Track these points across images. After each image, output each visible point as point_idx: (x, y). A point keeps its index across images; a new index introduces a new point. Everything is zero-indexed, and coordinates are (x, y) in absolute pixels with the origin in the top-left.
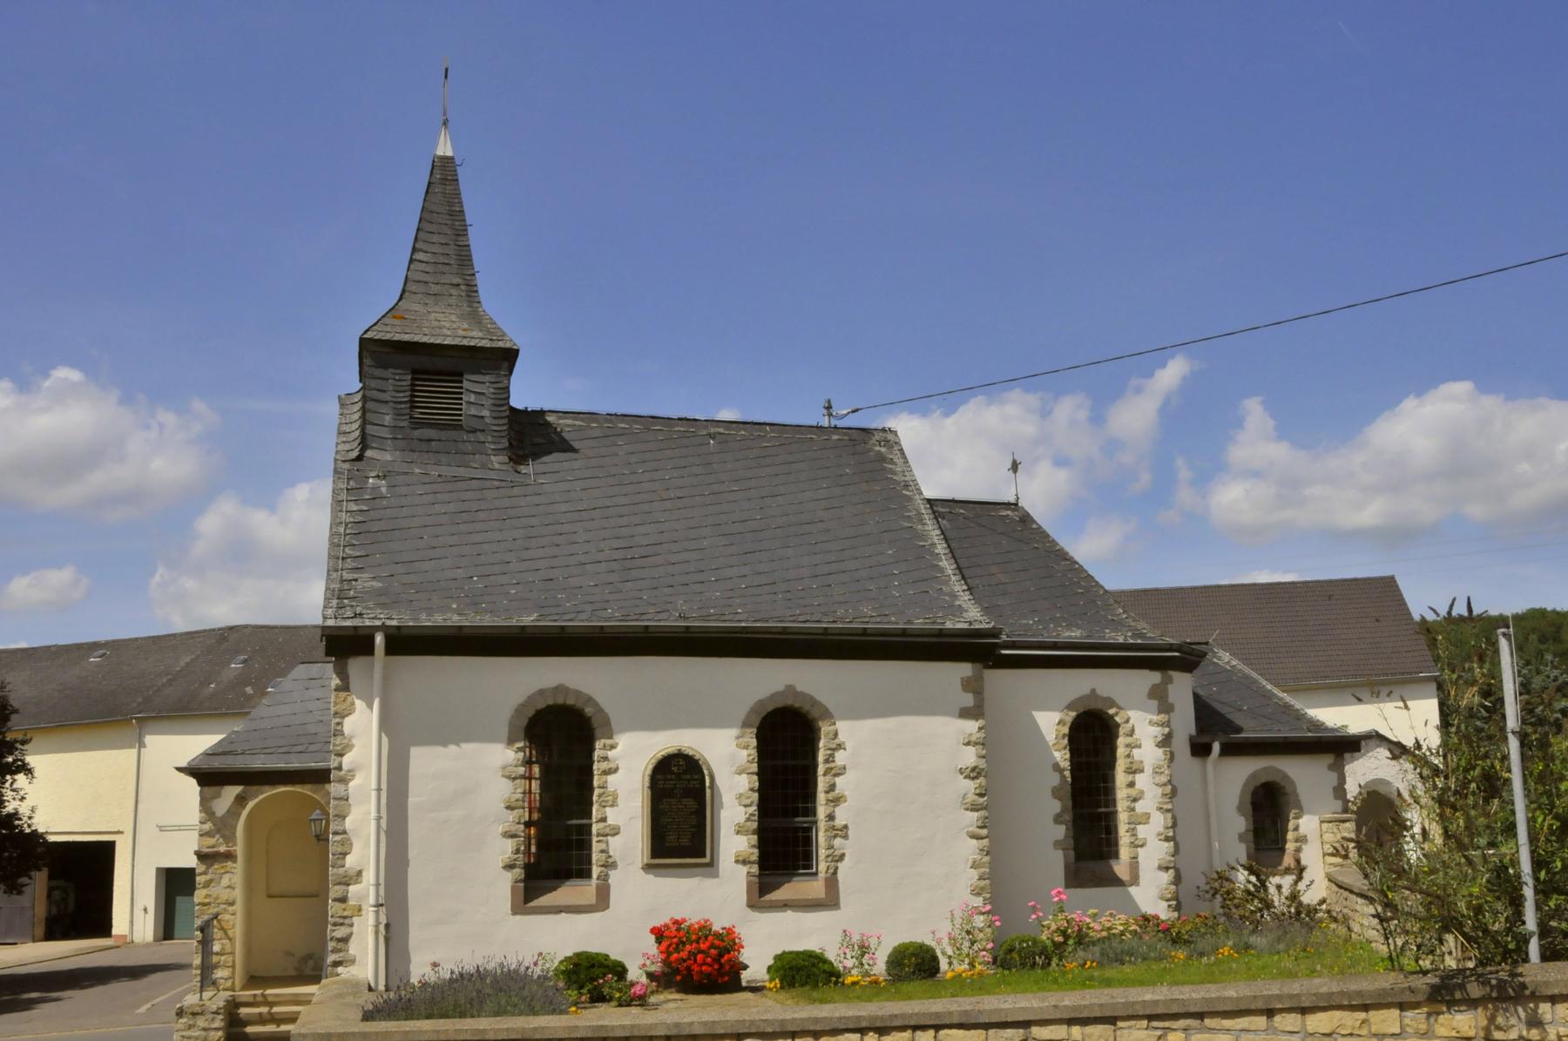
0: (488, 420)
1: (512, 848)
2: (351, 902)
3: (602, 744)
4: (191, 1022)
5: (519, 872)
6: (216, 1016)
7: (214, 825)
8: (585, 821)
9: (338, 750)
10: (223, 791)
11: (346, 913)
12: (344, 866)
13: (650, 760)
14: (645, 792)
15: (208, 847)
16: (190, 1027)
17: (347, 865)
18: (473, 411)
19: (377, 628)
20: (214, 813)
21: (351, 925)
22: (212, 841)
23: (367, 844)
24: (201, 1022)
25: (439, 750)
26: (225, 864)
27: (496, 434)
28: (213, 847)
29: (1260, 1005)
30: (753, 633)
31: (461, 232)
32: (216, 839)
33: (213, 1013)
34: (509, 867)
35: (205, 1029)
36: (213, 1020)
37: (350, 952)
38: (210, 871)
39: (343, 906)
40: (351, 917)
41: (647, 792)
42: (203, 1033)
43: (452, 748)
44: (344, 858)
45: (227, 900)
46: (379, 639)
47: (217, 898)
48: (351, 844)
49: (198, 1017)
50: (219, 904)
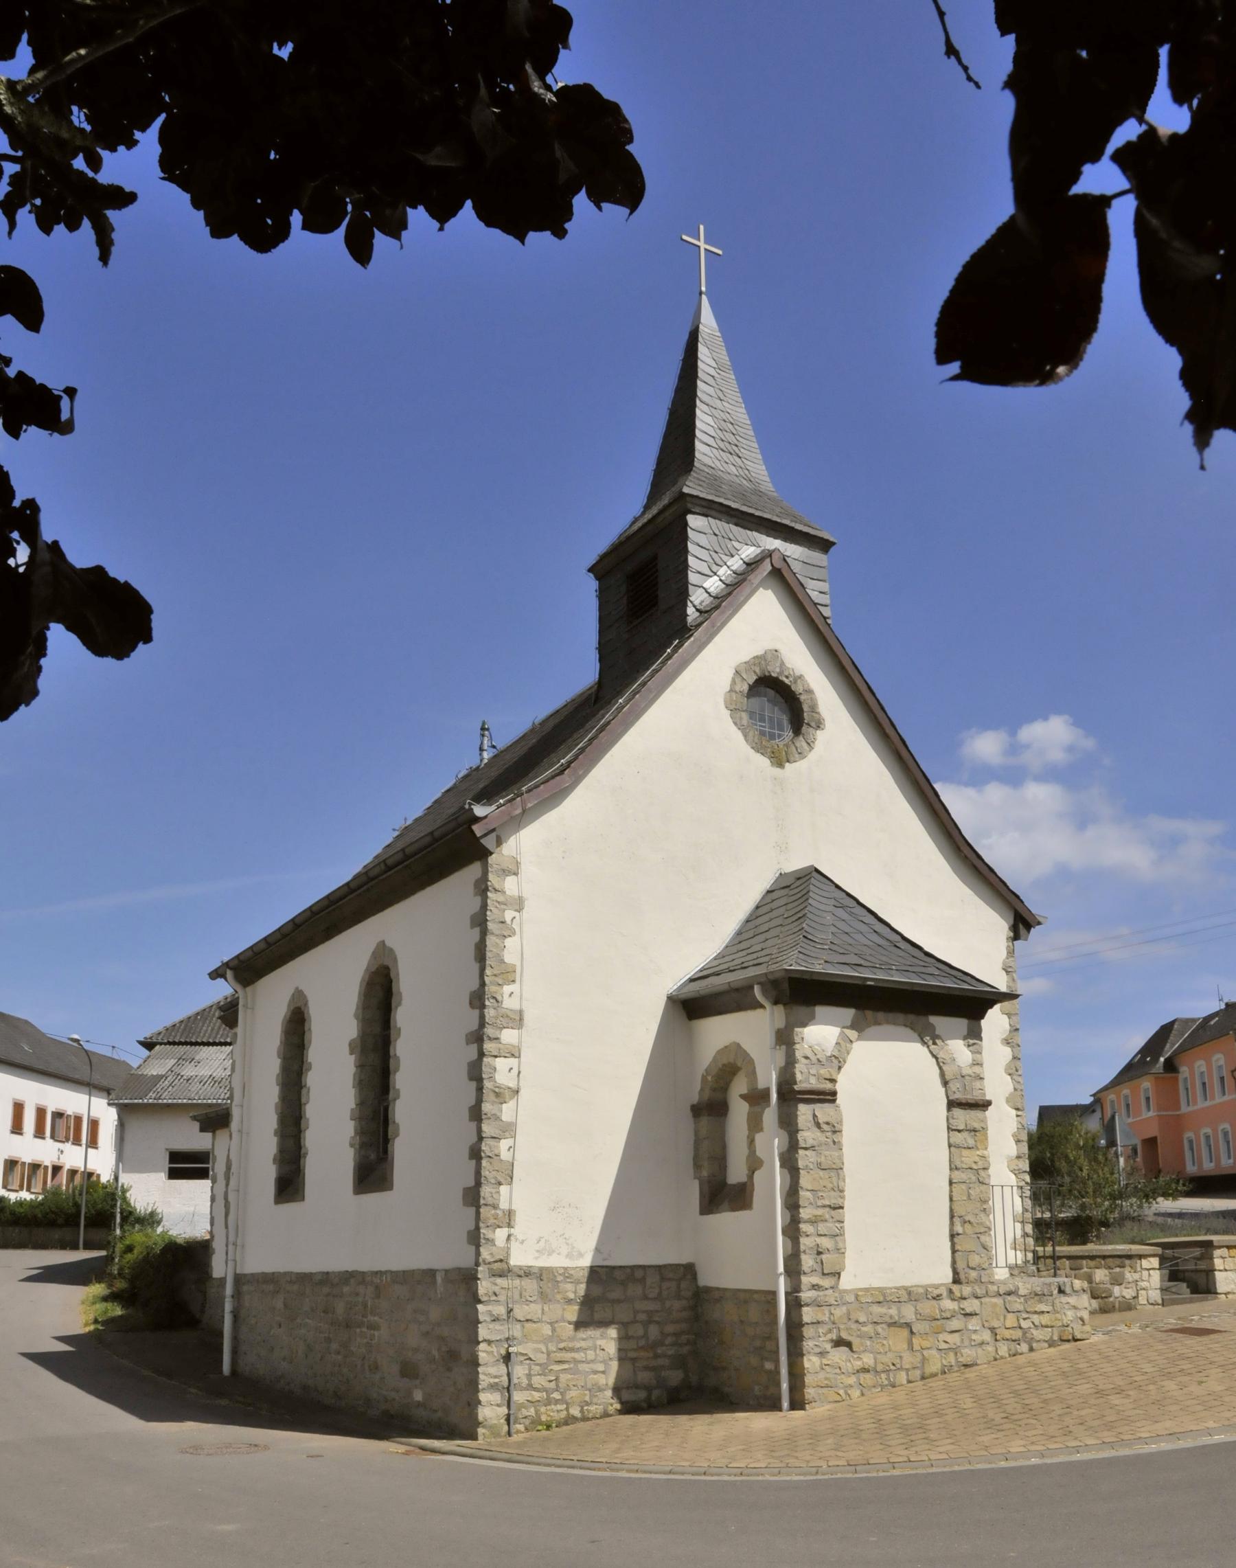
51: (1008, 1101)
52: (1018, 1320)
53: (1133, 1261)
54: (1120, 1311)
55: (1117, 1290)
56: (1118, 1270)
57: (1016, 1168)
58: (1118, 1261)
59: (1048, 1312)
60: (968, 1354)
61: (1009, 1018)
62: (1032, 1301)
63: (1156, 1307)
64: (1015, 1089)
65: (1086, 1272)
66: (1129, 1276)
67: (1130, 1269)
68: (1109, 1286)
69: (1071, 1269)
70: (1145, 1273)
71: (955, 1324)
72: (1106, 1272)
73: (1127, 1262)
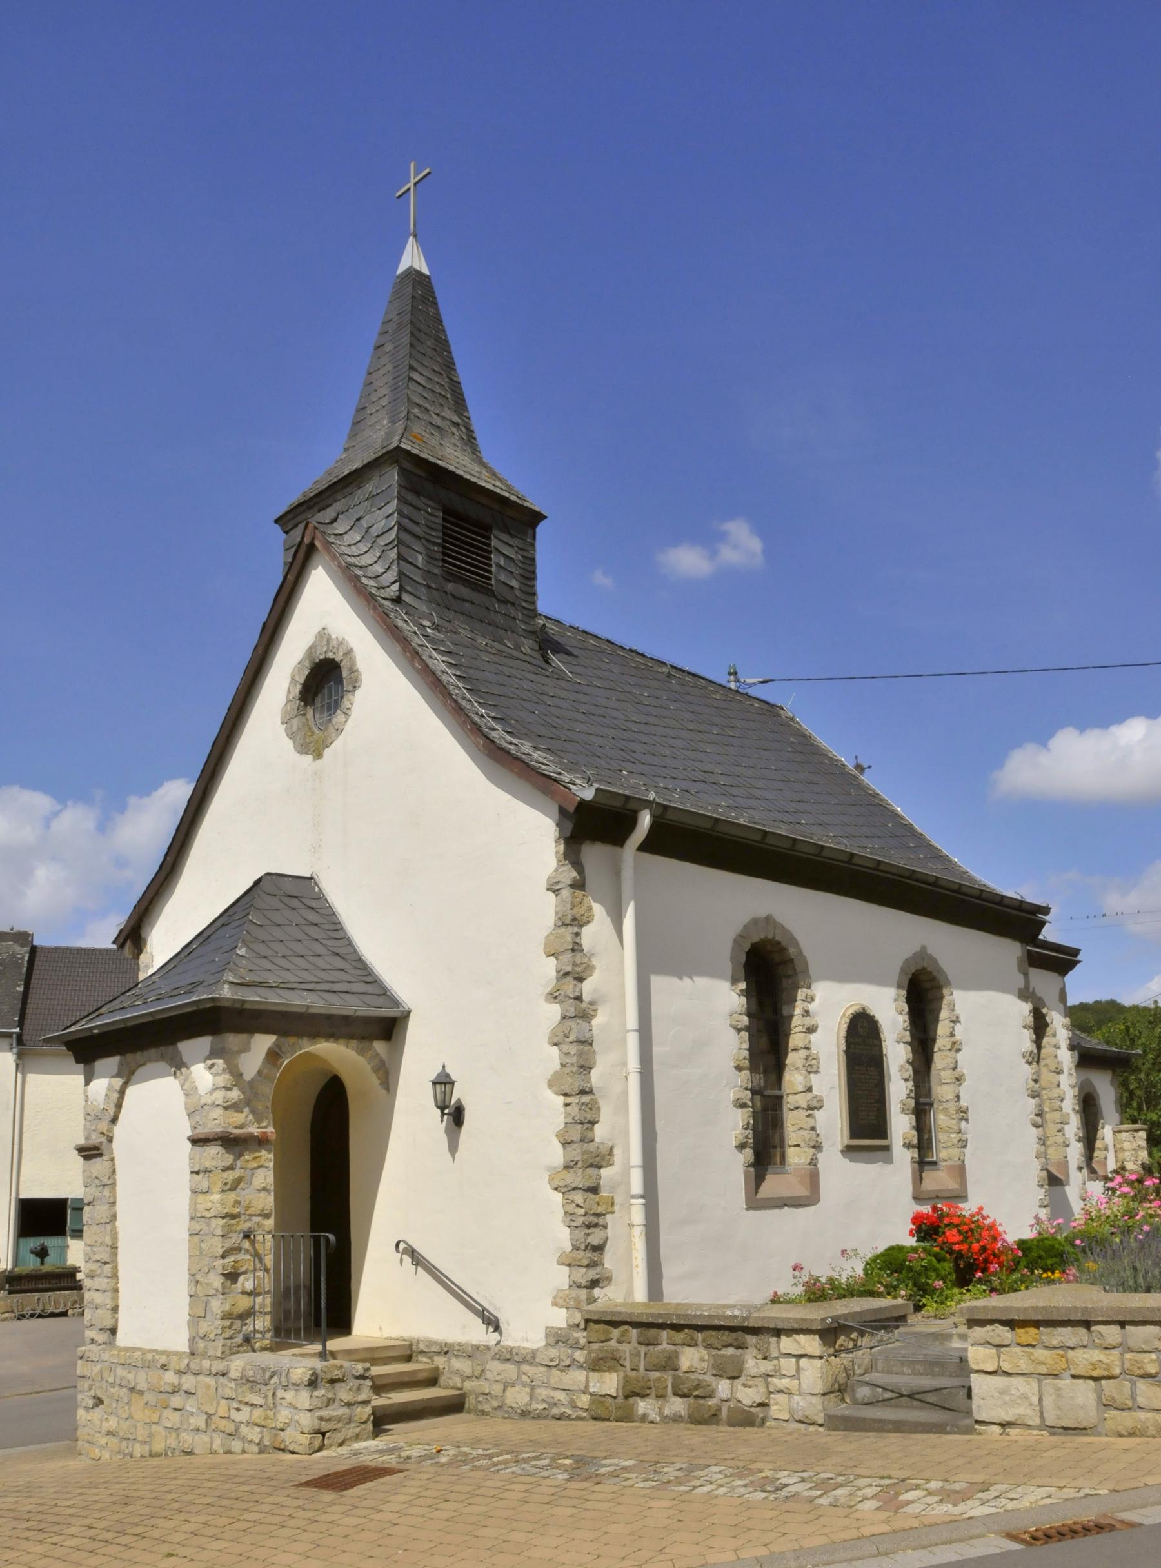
0: (518, 593)
1: (743, 1120)
2: (604, 1193)
3: (804, 995)
4: (330, 1395)
5: (749, 1153)
6: (362, 1382)
7: (243, 1093)
8: (777, 1092)
9: (578, 973)
10: (252, 1040)
11: (600, 1210)
12: (592, 1141)
13: (841, 1020)
14: (841, 1059)
15: (236, 1127)
16: (329, 1402)
17: (596, 1139)
18: (503, 577)
19: (648, 804)
20: (241, 1075)
21: (605, 1227)
22: (239, 1118)
23: (624, 1107)
24: (344, 1393)
25: (675, 981)
26: (257, 1154)
27: (525, 612)
28: (241, 1127)
29: (1079, 1317)
30: (917, 881)
31: (449, 365)
32: (244, 1115)
33: (357, 1378)
34: (741, 1147)
35: (349, 1404)
36: (359, 1389)
37: (606, 1266)
38: (239, 1163)
39: (597, 1198)
40: (604, 1215)
41: (843, 1057)
42: (346, 1410)
43: (686, 980)
44: (592, 1129)
45: (262, 1210)
46: (645, 820)
47: (248, 1207)
48: (599, 1109)
49: (338, 1385)
50: (250, 1215)
51: (550, 1085)
52: (229, 1410)
53: (765, 1337)
54: (730, 1424)
55: (723, 1388)
56: (730, 1351)
57: (562, 1184)
58: (726, 1337)
59: (261, 1406)
60: (187, 1439)
61: (557, 959)
62: (244, 1388)
63: (812, 1428)
64: (563, 1065)
65: (664, 1350)
66: (753, 1364)
67: (755, 1352)
68: (708, 1378)
69: (640, 1343)
70: (788, 1365)
71: (176, 1401)
72: (704, 1352)
73: (751, 1340)
